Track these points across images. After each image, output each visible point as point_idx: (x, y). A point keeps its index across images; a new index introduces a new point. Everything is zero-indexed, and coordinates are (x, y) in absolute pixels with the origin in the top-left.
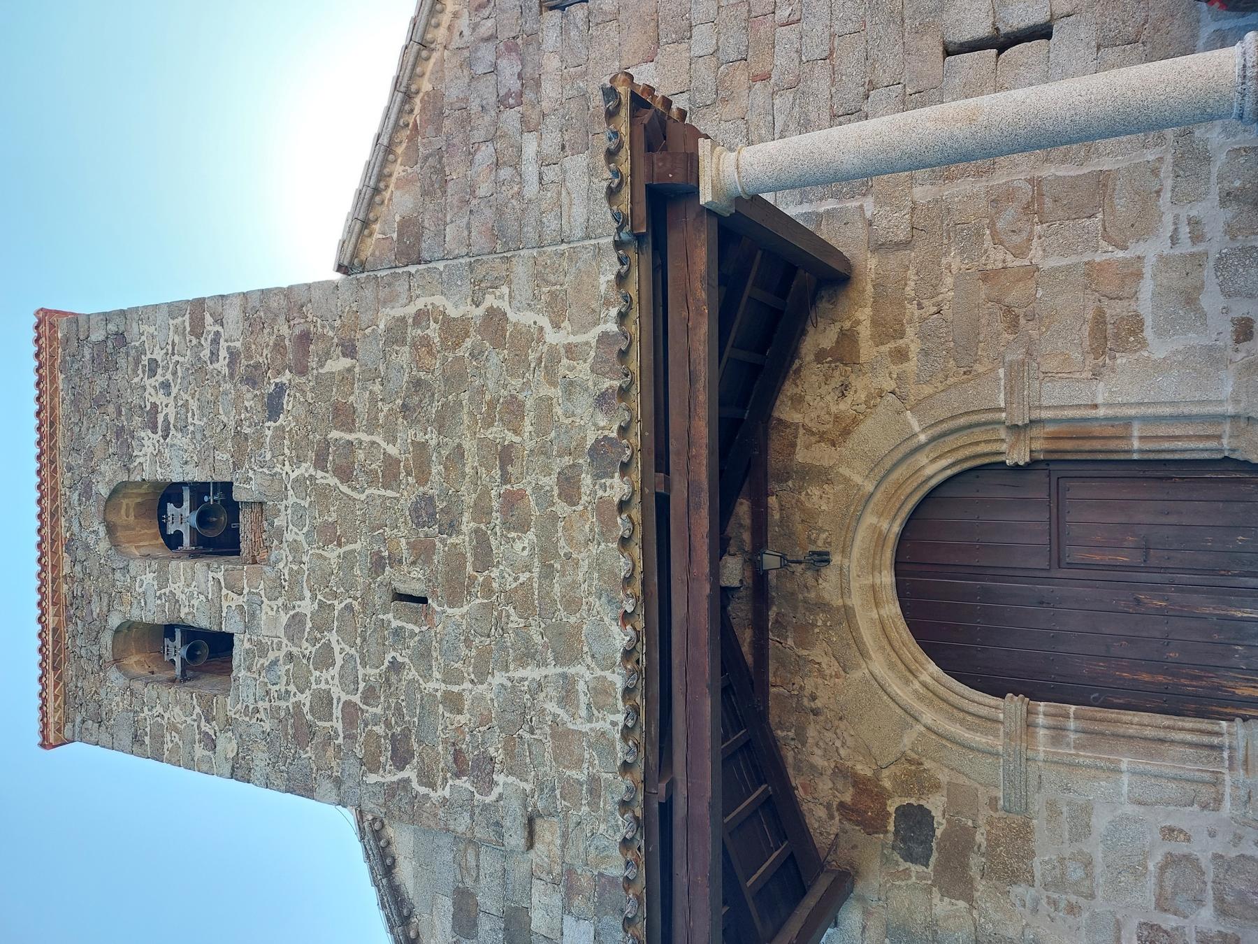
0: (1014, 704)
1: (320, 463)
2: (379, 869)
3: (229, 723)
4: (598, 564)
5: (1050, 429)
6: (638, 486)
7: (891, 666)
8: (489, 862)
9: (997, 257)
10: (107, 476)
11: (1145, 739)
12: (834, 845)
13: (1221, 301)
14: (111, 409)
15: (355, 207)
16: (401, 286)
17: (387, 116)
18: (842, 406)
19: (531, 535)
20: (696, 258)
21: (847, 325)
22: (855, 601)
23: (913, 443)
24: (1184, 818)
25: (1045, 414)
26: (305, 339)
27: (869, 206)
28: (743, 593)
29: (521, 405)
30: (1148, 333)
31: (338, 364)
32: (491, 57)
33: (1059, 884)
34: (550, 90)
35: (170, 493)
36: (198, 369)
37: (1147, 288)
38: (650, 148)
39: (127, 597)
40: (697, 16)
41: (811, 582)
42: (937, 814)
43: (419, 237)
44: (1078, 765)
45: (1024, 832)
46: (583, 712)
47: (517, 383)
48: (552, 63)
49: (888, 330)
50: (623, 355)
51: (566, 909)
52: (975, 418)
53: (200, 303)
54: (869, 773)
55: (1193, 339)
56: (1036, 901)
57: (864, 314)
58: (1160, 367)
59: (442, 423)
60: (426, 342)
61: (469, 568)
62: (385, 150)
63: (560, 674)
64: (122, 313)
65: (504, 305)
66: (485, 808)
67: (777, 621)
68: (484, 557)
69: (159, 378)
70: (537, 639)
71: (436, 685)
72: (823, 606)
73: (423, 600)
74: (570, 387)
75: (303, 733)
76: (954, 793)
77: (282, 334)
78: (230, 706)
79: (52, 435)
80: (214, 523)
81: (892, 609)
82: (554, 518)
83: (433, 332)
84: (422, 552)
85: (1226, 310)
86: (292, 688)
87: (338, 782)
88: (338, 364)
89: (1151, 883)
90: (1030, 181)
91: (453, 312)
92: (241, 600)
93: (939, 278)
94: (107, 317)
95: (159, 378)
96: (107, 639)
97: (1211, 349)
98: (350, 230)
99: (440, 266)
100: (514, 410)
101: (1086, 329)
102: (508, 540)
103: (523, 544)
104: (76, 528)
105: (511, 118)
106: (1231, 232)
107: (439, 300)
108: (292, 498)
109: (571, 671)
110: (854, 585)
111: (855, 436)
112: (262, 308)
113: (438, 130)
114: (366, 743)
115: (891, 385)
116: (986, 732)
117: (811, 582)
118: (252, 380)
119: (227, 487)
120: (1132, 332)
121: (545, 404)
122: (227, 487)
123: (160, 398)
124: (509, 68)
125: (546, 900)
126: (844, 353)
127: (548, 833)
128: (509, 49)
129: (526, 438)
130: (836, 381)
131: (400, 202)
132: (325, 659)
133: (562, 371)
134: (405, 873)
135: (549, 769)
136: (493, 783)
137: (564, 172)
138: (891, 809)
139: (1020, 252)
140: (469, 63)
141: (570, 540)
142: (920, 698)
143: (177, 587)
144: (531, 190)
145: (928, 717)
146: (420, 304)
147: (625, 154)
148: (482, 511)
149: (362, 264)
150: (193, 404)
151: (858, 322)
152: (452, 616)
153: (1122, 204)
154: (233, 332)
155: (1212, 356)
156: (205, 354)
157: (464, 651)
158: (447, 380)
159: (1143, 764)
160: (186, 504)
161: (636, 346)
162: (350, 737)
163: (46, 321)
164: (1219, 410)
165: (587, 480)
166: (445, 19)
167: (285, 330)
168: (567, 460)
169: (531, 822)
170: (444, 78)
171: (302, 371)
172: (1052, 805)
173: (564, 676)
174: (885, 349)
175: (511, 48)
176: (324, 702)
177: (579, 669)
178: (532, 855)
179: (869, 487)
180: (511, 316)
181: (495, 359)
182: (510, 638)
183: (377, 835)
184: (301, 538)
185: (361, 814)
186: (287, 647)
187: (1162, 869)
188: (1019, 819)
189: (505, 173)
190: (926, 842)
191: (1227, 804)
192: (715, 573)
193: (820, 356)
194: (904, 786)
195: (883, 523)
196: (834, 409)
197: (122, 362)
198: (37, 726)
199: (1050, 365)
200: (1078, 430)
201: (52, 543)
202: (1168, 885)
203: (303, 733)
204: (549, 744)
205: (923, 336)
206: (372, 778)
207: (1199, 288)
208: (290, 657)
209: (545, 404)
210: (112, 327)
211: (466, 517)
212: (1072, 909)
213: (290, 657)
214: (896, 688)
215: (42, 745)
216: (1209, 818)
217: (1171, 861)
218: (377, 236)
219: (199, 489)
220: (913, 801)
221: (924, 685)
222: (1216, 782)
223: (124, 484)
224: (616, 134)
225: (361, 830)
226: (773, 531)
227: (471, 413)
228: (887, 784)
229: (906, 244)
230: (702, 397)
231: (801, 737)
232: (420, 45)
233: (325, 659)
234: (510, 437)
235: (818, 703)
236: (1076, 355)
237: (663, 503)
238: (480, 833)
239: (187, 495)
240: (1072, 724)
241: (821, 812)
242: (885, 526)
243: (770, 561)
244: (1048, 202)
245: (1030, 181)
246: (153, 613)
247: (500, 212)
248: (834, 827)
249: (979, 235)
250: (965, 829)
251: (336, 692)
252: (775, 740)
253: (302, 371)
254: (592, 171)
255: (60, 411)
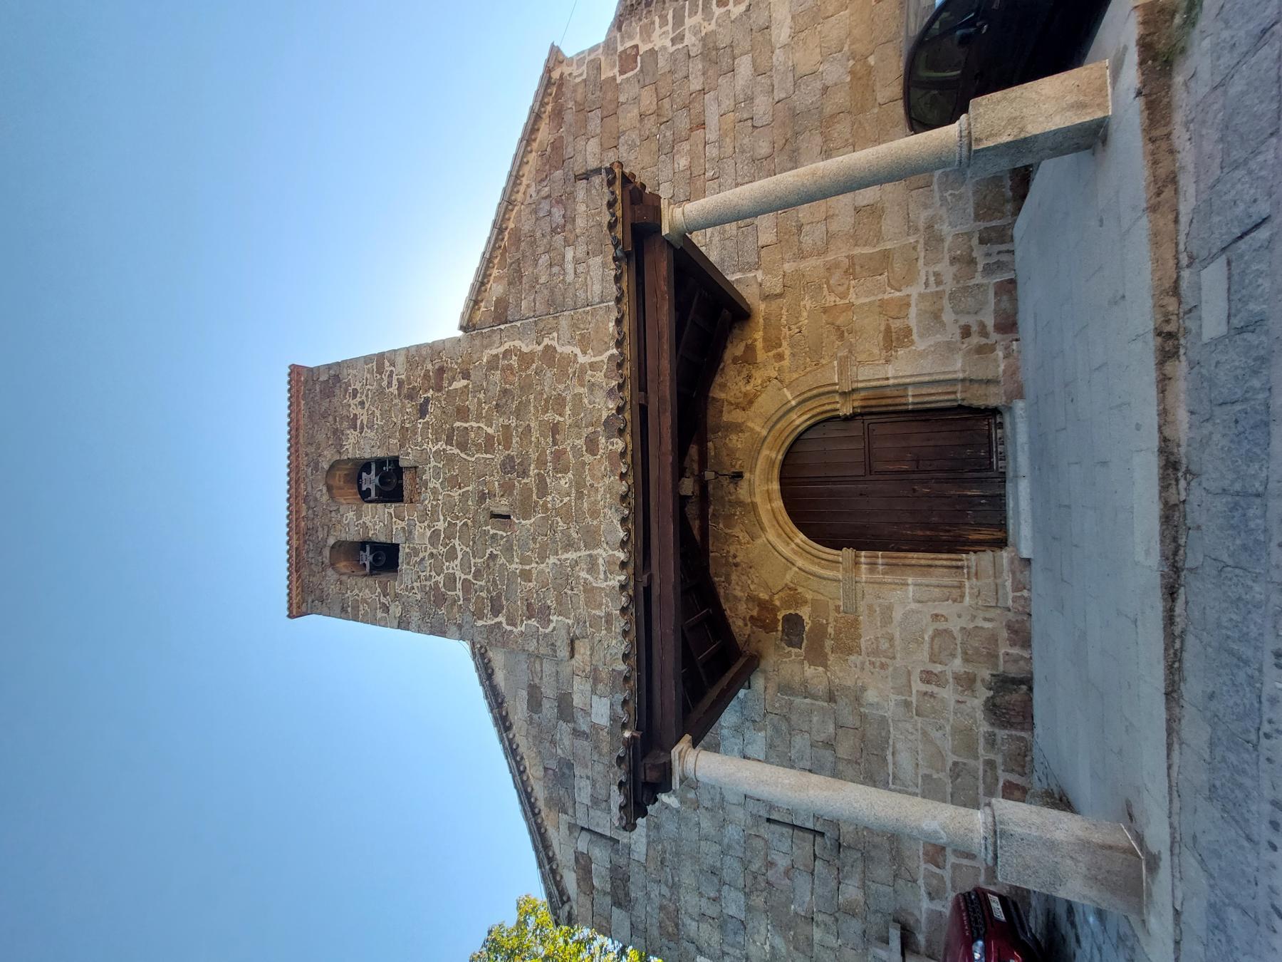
0: (848, 553)
1: (449, 441)
2: (484, 676)
3: (397, 595)
4: (609, 489)
5: (863, 394)
6: (628, 399)
7: (779, 536)
8: (548, 667)
9: (831, 300)
10: (329, 456)
11: (921, 566)
12: (747, 642)
13: (953, 317)
14: (331, 418)
15: (470, 293)
16: (496, 338)
17: (489, 242)
18: (748, 388)
19: (570, 475)
20: (661, 269)
21: (750, 342)
22: (758, 499)
23: (789, 406)
24: (945, 608)
25: (860, 385)
26: (441, 371)
27: (760, 275)
28: (694, 499)
29: (564, 399)
30: (915, 337)
31: (460, 384)
32: (547, 208)
33: (876, 652)
34: (580, 222)
35: (365, 466)
36: (381, 393)
37: (913, 311)
38: (633, 203)
39: (338, 527)
40: (661, 179)
41: (732, 490)
42: (806, 618)
43: (506, 309)
44: (885, 583)
45: (855, 624)
46: (602, 576)
47: (561, 387)
48: (582, 208)
49: (773, 343)
50: (620, 366)
51: (594, 692)
52: (821, 390)
53: (381, 357)
54: (767, 598)
55: (939, 338)
56: (863, 663)
57: (759, 335)
58: (922, 355)
59: (518, 414)
60: (510, 367)
61: (535, 497)
62: (488, 262)
63: (587, 563)
64: (338, 364)
65: (555, 343)
66: (545, 635)
67: (714, 515)
68: (543, 489)
69: (358, 399)
70: (575, 535)
71: (515, 566)
72: (740, 503)
73: (508, 517)
74: (592, 387)
75: (440, 599)
76: (815, 604)
77: (428, 372)
78: (397, 586)
79: (297, 436)
80: (389, 481)
81: (779, 504)
82: (584, 464)
83: (514, 361)
84: (507, 489)
85: (956, 321)
86: (433, 573)
87: (460, 627)
88: (460, 384)
89: (926, 646)
90: (847, 257)
91: (525, 349)
92: (403, 524)
93: (800, 313)
94: (329, 367)
95: (358, 399)
96: (327, 552)
97: (948, 343)
98: (467, 306)
99: (518, 324)
100: (560, 402)
101: (881, 336)
102: (557, 479)
103: (565, 482)
104: (309, 489)
105: (559, 239)
106: (956, 278)
107: (517, 343)
108: (433, 464)
109: (595, 552)
110: (757, 491)
111: (756, 404)
112: (415, 356)
113: (518, 249)
114: (476, 603)
115: (776, 374)
116: (832, 569)
117: (732, 490)
118: (410, 397)
119: (395, 460)
120: (906, 337)
121: (578, 397)
122: (395, 460)
123: (359, 411)
124: (558, 213)
125: (581, 687)
126: (749, 358)
127: (583, 648)
128: (558, 202)
129: (567, 418)
130: (745, 373)
131: (496, 289)
132: (452, 555)
133: (587, 378)
134: (499, 677)
135: (582, 611)
136: (550, 621)
137: (589, 267)
138: (780, 617)
139: (843, 296)
140: (535, 211)
141: (593, 477)
142: (795, 553)
143: (367, 519)
144: (570, 277)
145: (800, 563)
146: (506, 346)
147: (619, 205)
148: (541, 463)
149: (474, 325)
150: (378, 413)
151: (756, 340)
152: (526, 524)
153: (898, 266)
154: (401, 371)
155: (950, 347)
156: (385, 384)
157: (532, 545)
158: (522, 388)
159: (920, 580)
160: (373, 472)
161: (627, 317)
162: (466, 600)
163: (295, 371)
164: (954, 376)
165: (602, 440)
166: (522, 188)
167: (430, 367)
168: (591, 429)
169: (572, 642)
170: (522, 220)
171: (439, 388)
172: (870, 607)
173: (590, 556)
174: (771, 354)
175: (559, 201)
176: (451, 579)
177: (600, 551)
178: (573, 661)
179: (764, 433)
180: (559, 349)
181: (549, 374)
182: (558, 536)
183: (483, 656)
184: (438, 486)
185: (473, 645)
186: (430, 549)
187: (933, 639)
188: (852, 617)
189: (555, 269)
190: (800, 635)
191: (967, 598)
192: (676, 486)
193: (735, 360)
194: (787, 603)
195: (772, 454)
196: (743, 390)
197: (337, 391)
198: (286, 605)
199: (861, 357)
200: (878, 391)
201: (297, 497)
202: (936, 647)
203: (440, 599)
204: (582, 597)
205: (792, 346)
206: (480, 623)
207: (941, 310)
208: (432, 555)
209: (578, 397)
210: (332, 372)
211: (532, 467)
212: (883, 666)
213: (432, 555)
214: (781, 547)
215: (289, 616)
216: (956, 608)
217: (937, 633)
218: (483, 309)
219: (380, 462)
220: (792, 611)
221: (798, 545)
222: (961, 586)
223: (337, 462)
224: (613, 193)
225: (474, 654)
226: (711, 462)
227: (535, 407)
228: (777, 603)
229: (780, 295)
230: (666, 347)
231: (728, 580)
232: (508, 203)
233: (452, 555)
234: (558, 418)
235: (738, 560)
236: (876, 351)
237: (643, 410)
238: (543, 650)
239: (373, 467)
240: (880, 561)
241: (740, 623)
242: (774, 455)
243: (709, 475)
244: (858, 268)
245: (847, 257)
246: (353, 535)
247: (552, 292)
248: (747, 631)
249: (821, 288)
250: (822, 625)
251: (458, 574)
252: (713, 583)
253: (439, 388)
254: (604, 265)
255: (302, 422)
